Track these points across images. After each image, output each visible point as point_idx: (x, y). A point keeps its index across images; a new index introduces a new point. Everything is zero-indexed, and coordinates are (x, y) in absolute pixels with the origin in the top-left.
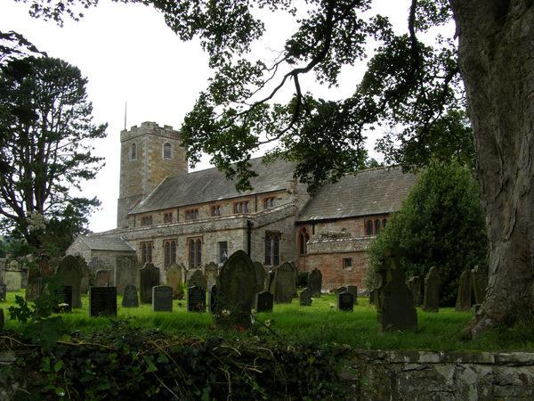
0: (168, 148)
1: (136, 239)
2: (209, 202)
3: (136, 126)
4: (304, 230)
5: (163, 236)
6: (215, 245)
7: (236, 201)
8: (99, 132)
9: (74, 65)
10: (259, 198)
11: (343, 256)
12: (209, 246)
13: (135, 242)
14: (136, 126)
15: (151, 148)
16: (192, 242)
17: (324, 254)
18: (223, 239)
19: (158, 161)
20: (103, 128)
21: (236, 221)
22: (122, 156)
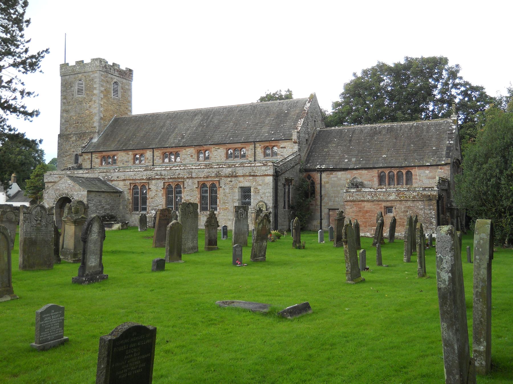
0: (115, 86)
1: (124, 180)
2: (397, 167)
3: (82, 61)
4: (309, 177)
5: (164, 179)
6: (236, 190)
7: (229, 146)
8: (31, 64)
9: (374, 64)
10: (257, 145)
11: (384, 204)
12: (227, 191)
13: (121, 183)
14: (82, 61)
15: (102, 86)
16: (203, 185)
17: (363, 201)
18: (246, 184)
19: (108, 100)
20: (39, 56)
21: (264, 168)
22: (62, 91)
